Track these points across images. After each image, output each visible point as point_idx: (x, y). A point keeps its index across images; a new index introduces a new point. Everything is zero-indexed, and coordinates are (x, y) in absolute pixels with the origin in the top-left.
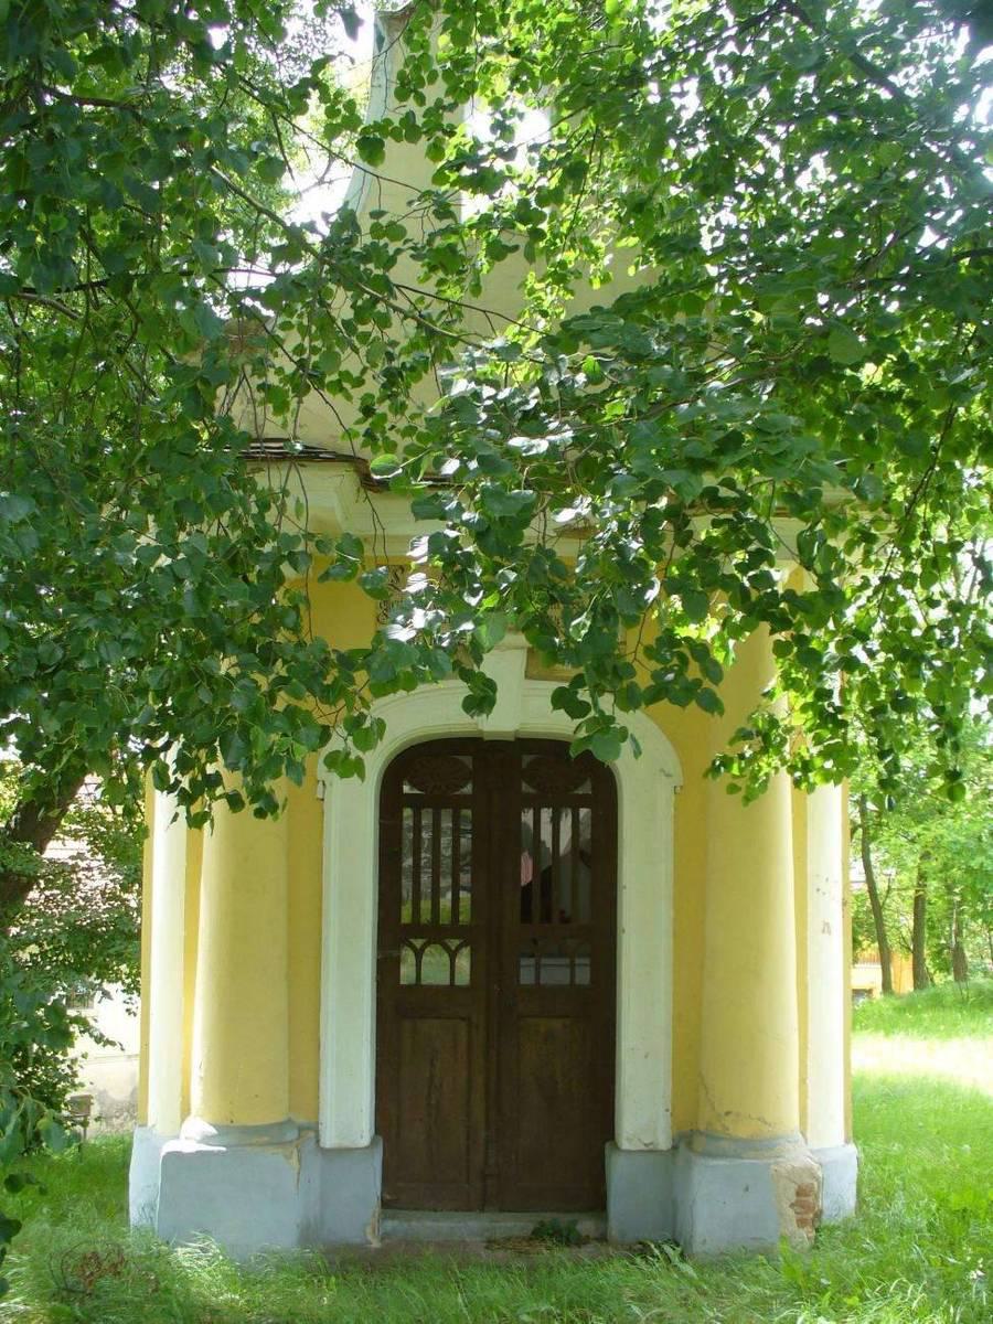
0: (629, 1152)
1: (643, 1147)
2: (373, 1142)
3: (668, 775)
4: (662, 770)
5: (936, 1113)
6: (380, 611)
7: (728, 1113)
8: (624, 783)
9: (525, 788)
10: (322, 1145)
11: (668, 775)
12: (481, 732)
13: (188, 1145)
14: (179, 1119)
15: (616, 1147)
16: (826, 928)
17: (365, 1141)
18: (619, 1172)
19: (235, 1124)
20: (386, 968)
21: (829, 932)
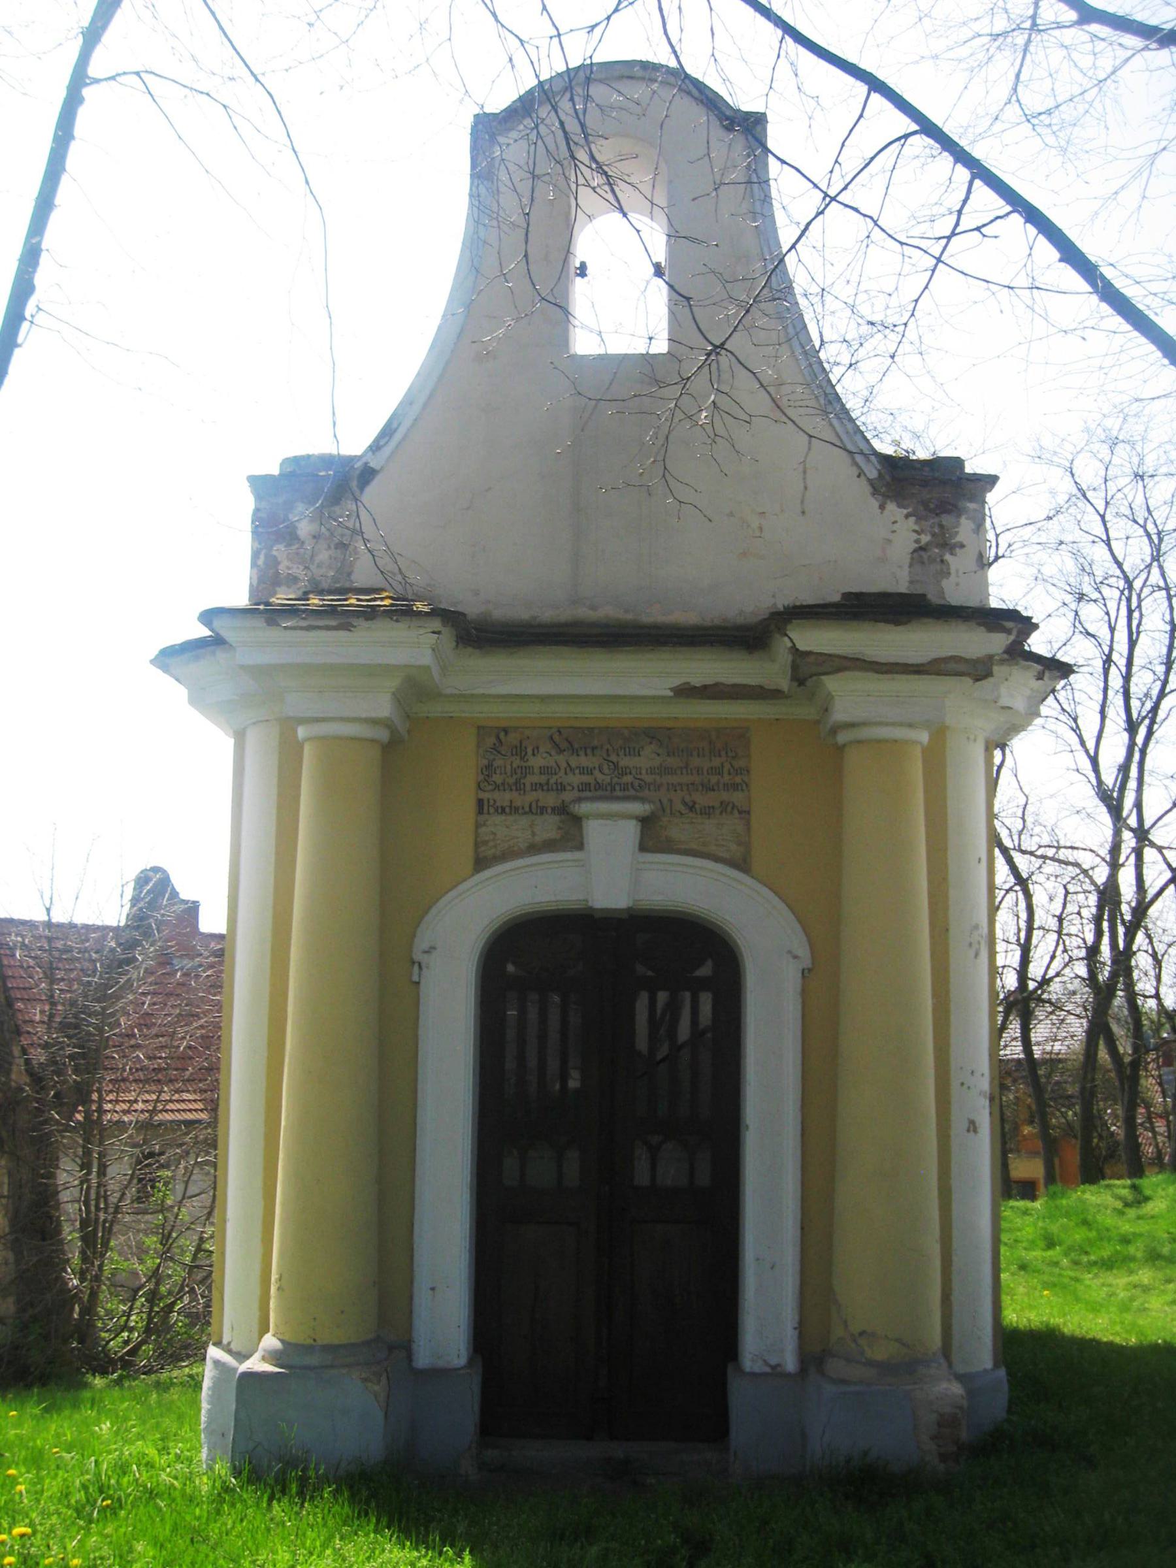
0: (753, 1375)
1: (768, 1370)
2: (470, 1363)
3: (795, 957)
4: (789, 952)
5: (95, 1064)
6: (481, 777)
7: (774, 596)
8: (748, 971)
9: (640, 969)
10: (414, 1364)
11: (795, 957)
12: (591, 908)
13: (256, 1364)
14: (256, 1335)
15: (739, 1369)
16: (973, 1127)
17: (463, 1361)
18: (740, 1396)
19: (319, 1342)
20: (214, 1107)
21: (975, 1131)
